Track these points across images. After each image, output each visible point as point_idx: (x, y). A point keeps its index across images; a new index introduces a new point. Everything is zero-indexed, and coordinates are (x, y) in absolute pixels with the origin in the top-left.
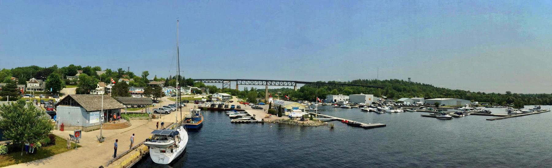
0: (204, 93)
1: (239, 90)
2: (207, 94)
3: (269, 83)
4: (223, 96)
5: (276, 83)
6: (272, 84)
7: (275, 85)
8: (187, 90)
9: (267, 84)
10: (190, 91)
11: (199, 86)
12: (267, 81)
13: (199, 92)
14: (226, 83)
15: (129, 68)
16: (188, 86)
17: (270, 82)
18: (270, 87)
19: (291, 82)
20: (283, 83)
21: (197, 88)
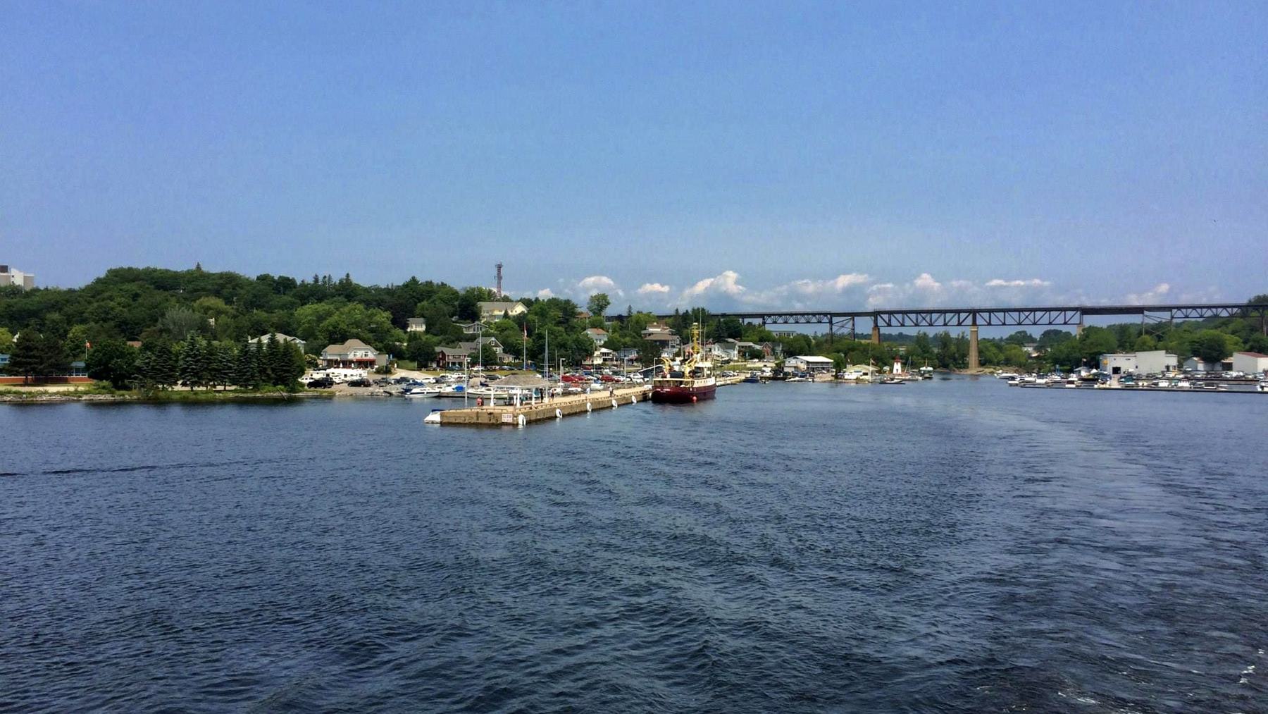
0: (770, 357)
1: (276, 278)
2: (776, 359)
3: (936, 321)
4: (808, 363)
5: (906, 319)
8: (729, 351)
9: (974, 324)
10: (736, 352)
11: (756, 338)
12: (974, 312)
13: (758, 356)
14: (840, 324)
15: (499, 267)
16: (731, 340)
17: (886, 317)
18: (986, 333)
21: (751, 344)
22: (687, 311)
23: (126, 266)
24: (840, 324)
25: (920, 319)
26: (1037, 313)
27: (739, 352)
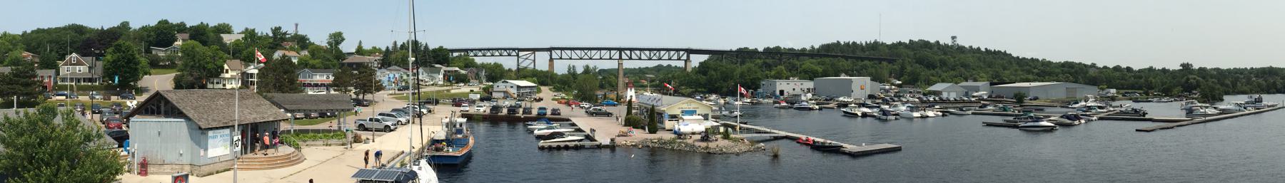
2: (481, 83)
4: (519, 87)
5: (642, 54)
6: (633, 58)
7: (640, 59)
8: (433, 75)
10: (441, 76)
15: (297, 25)
16: (437, 66)
17: (628, 52)
19: (678, 50)
20: (657, 54)
21: (457, 69)
22: (404, 43)
23: (112, 27)
24: (525, 57)
25: (583, 54)
26: (592, 51)
27: (444, 76)
